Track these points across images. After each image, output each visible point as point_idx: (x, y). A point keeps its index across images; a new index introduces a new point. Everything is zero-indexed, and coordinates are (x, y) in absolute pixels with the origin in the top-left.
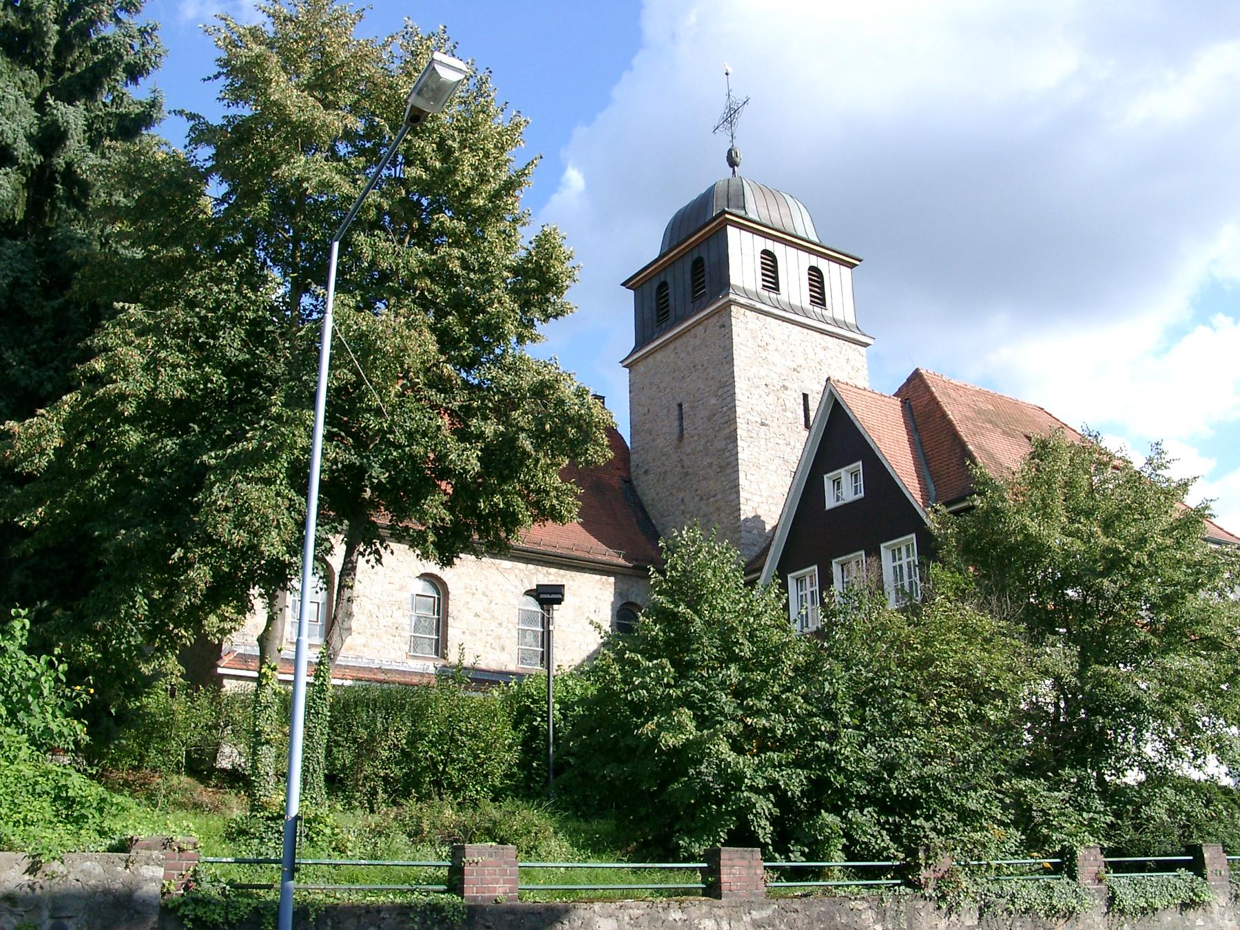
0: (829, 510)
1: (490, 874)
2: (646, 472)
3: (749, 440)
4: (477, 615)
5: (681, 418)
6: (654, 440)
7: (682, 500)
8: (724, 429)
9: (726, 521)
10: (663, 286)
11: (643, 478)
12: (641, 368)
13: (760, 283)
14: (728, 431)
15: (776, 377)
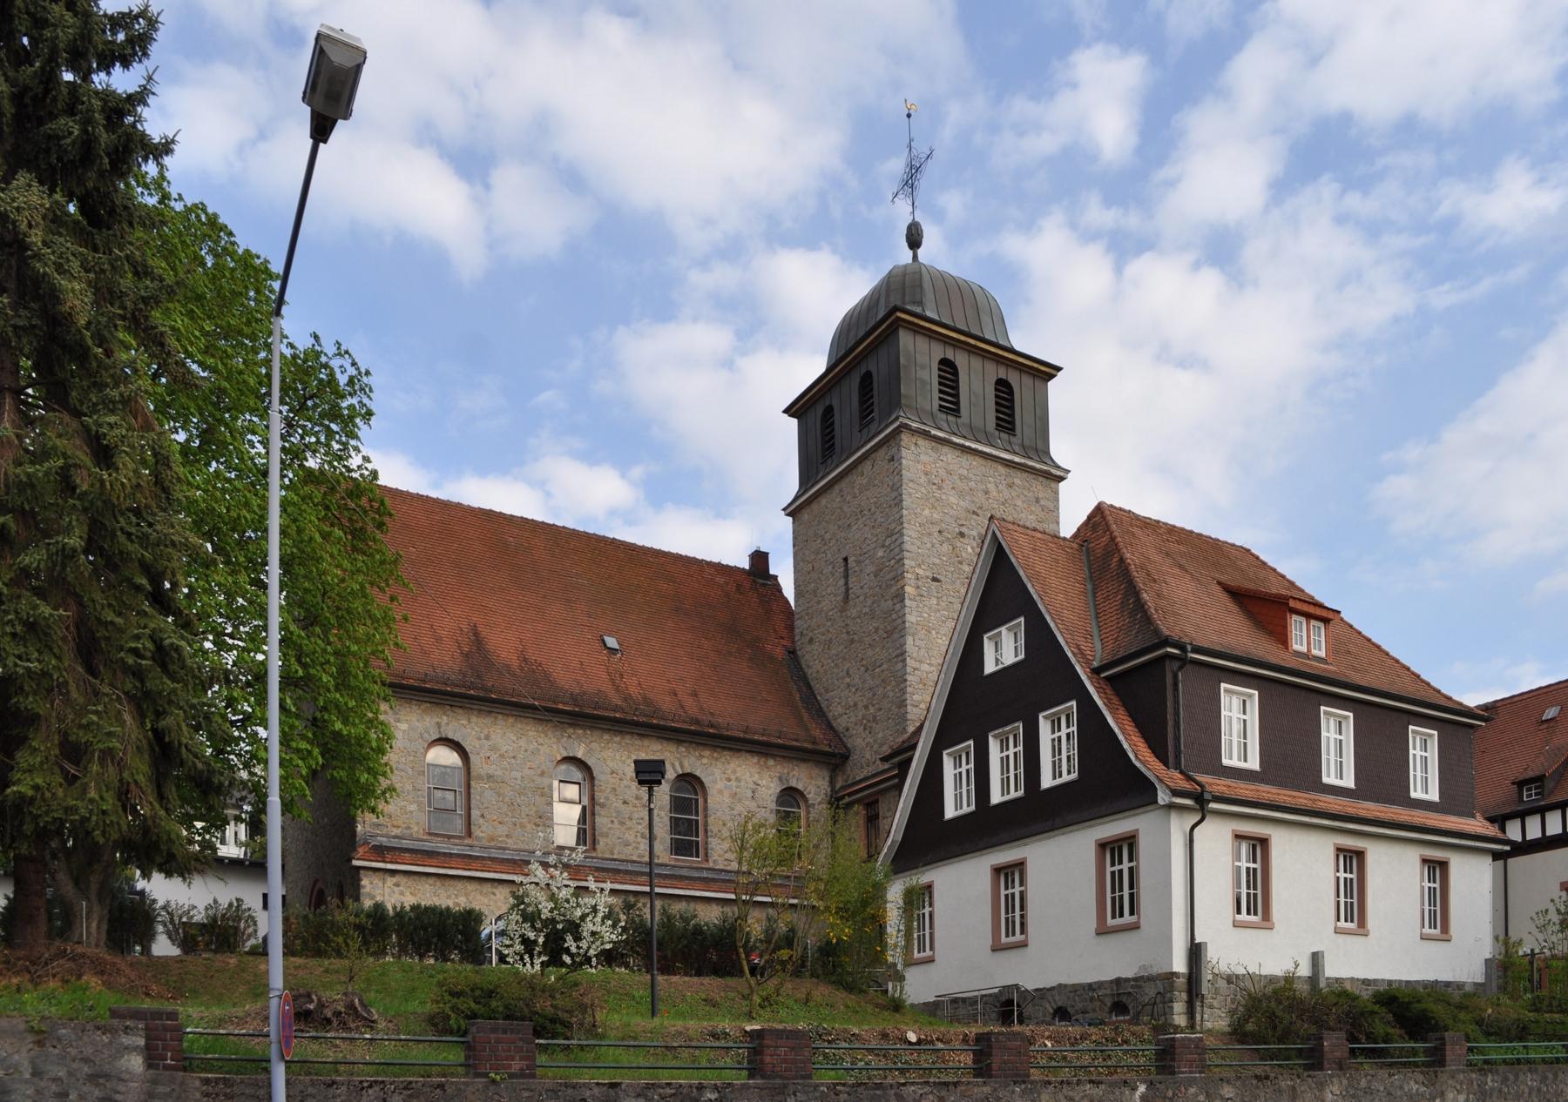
0: (1356, 785)
1: (504, 1051)
2: (811, 641)
3: (917, 598)
4: (625, 802)
5: (846, 577)
6: (819, 602)
7: (848, 673)
8: (892, 586)
9: (891, 694)
10: (829, 410)
11: (809, 648)
12: (805, 516)
13: (936, 403)
14: (894, 588)
15: (951, 520)
